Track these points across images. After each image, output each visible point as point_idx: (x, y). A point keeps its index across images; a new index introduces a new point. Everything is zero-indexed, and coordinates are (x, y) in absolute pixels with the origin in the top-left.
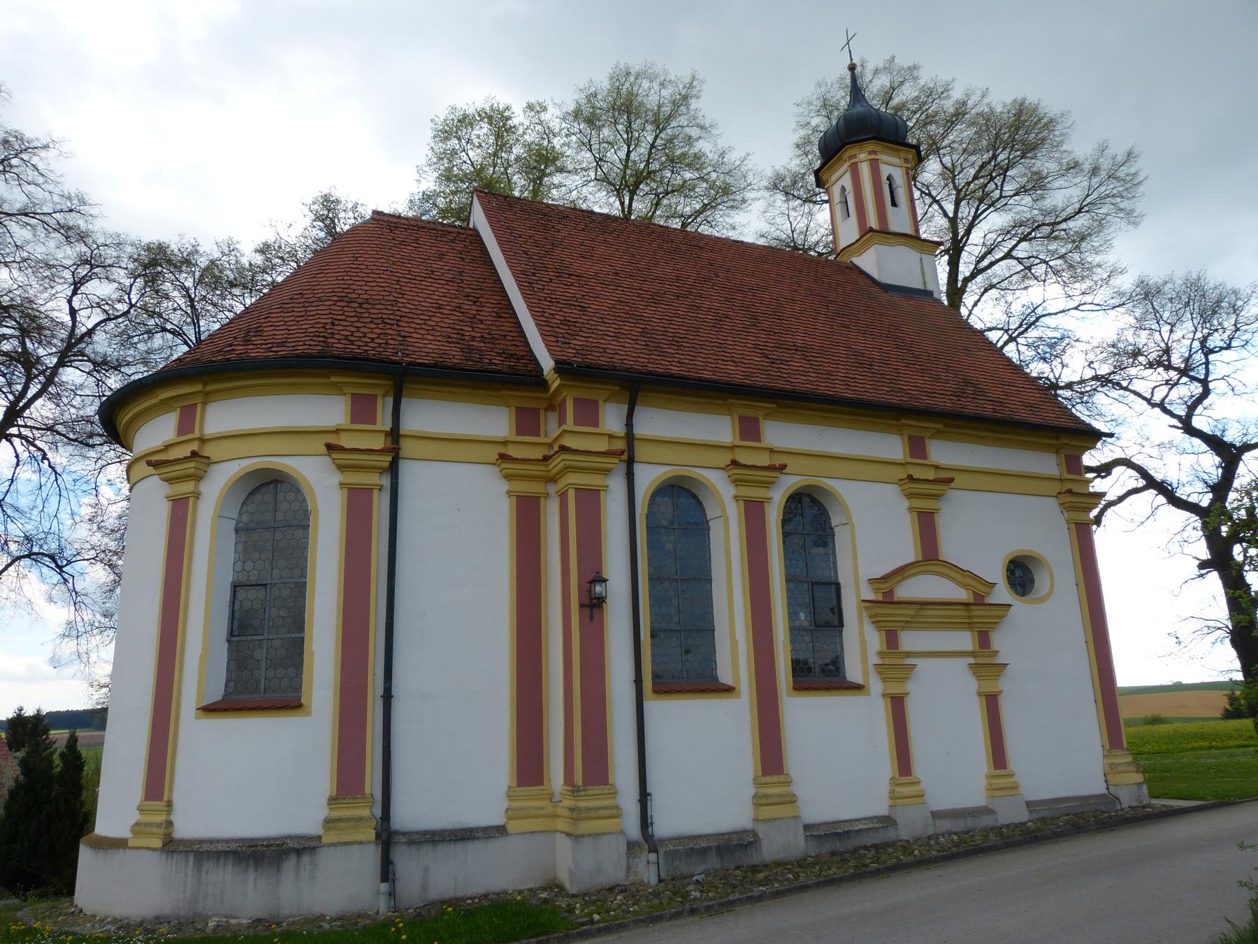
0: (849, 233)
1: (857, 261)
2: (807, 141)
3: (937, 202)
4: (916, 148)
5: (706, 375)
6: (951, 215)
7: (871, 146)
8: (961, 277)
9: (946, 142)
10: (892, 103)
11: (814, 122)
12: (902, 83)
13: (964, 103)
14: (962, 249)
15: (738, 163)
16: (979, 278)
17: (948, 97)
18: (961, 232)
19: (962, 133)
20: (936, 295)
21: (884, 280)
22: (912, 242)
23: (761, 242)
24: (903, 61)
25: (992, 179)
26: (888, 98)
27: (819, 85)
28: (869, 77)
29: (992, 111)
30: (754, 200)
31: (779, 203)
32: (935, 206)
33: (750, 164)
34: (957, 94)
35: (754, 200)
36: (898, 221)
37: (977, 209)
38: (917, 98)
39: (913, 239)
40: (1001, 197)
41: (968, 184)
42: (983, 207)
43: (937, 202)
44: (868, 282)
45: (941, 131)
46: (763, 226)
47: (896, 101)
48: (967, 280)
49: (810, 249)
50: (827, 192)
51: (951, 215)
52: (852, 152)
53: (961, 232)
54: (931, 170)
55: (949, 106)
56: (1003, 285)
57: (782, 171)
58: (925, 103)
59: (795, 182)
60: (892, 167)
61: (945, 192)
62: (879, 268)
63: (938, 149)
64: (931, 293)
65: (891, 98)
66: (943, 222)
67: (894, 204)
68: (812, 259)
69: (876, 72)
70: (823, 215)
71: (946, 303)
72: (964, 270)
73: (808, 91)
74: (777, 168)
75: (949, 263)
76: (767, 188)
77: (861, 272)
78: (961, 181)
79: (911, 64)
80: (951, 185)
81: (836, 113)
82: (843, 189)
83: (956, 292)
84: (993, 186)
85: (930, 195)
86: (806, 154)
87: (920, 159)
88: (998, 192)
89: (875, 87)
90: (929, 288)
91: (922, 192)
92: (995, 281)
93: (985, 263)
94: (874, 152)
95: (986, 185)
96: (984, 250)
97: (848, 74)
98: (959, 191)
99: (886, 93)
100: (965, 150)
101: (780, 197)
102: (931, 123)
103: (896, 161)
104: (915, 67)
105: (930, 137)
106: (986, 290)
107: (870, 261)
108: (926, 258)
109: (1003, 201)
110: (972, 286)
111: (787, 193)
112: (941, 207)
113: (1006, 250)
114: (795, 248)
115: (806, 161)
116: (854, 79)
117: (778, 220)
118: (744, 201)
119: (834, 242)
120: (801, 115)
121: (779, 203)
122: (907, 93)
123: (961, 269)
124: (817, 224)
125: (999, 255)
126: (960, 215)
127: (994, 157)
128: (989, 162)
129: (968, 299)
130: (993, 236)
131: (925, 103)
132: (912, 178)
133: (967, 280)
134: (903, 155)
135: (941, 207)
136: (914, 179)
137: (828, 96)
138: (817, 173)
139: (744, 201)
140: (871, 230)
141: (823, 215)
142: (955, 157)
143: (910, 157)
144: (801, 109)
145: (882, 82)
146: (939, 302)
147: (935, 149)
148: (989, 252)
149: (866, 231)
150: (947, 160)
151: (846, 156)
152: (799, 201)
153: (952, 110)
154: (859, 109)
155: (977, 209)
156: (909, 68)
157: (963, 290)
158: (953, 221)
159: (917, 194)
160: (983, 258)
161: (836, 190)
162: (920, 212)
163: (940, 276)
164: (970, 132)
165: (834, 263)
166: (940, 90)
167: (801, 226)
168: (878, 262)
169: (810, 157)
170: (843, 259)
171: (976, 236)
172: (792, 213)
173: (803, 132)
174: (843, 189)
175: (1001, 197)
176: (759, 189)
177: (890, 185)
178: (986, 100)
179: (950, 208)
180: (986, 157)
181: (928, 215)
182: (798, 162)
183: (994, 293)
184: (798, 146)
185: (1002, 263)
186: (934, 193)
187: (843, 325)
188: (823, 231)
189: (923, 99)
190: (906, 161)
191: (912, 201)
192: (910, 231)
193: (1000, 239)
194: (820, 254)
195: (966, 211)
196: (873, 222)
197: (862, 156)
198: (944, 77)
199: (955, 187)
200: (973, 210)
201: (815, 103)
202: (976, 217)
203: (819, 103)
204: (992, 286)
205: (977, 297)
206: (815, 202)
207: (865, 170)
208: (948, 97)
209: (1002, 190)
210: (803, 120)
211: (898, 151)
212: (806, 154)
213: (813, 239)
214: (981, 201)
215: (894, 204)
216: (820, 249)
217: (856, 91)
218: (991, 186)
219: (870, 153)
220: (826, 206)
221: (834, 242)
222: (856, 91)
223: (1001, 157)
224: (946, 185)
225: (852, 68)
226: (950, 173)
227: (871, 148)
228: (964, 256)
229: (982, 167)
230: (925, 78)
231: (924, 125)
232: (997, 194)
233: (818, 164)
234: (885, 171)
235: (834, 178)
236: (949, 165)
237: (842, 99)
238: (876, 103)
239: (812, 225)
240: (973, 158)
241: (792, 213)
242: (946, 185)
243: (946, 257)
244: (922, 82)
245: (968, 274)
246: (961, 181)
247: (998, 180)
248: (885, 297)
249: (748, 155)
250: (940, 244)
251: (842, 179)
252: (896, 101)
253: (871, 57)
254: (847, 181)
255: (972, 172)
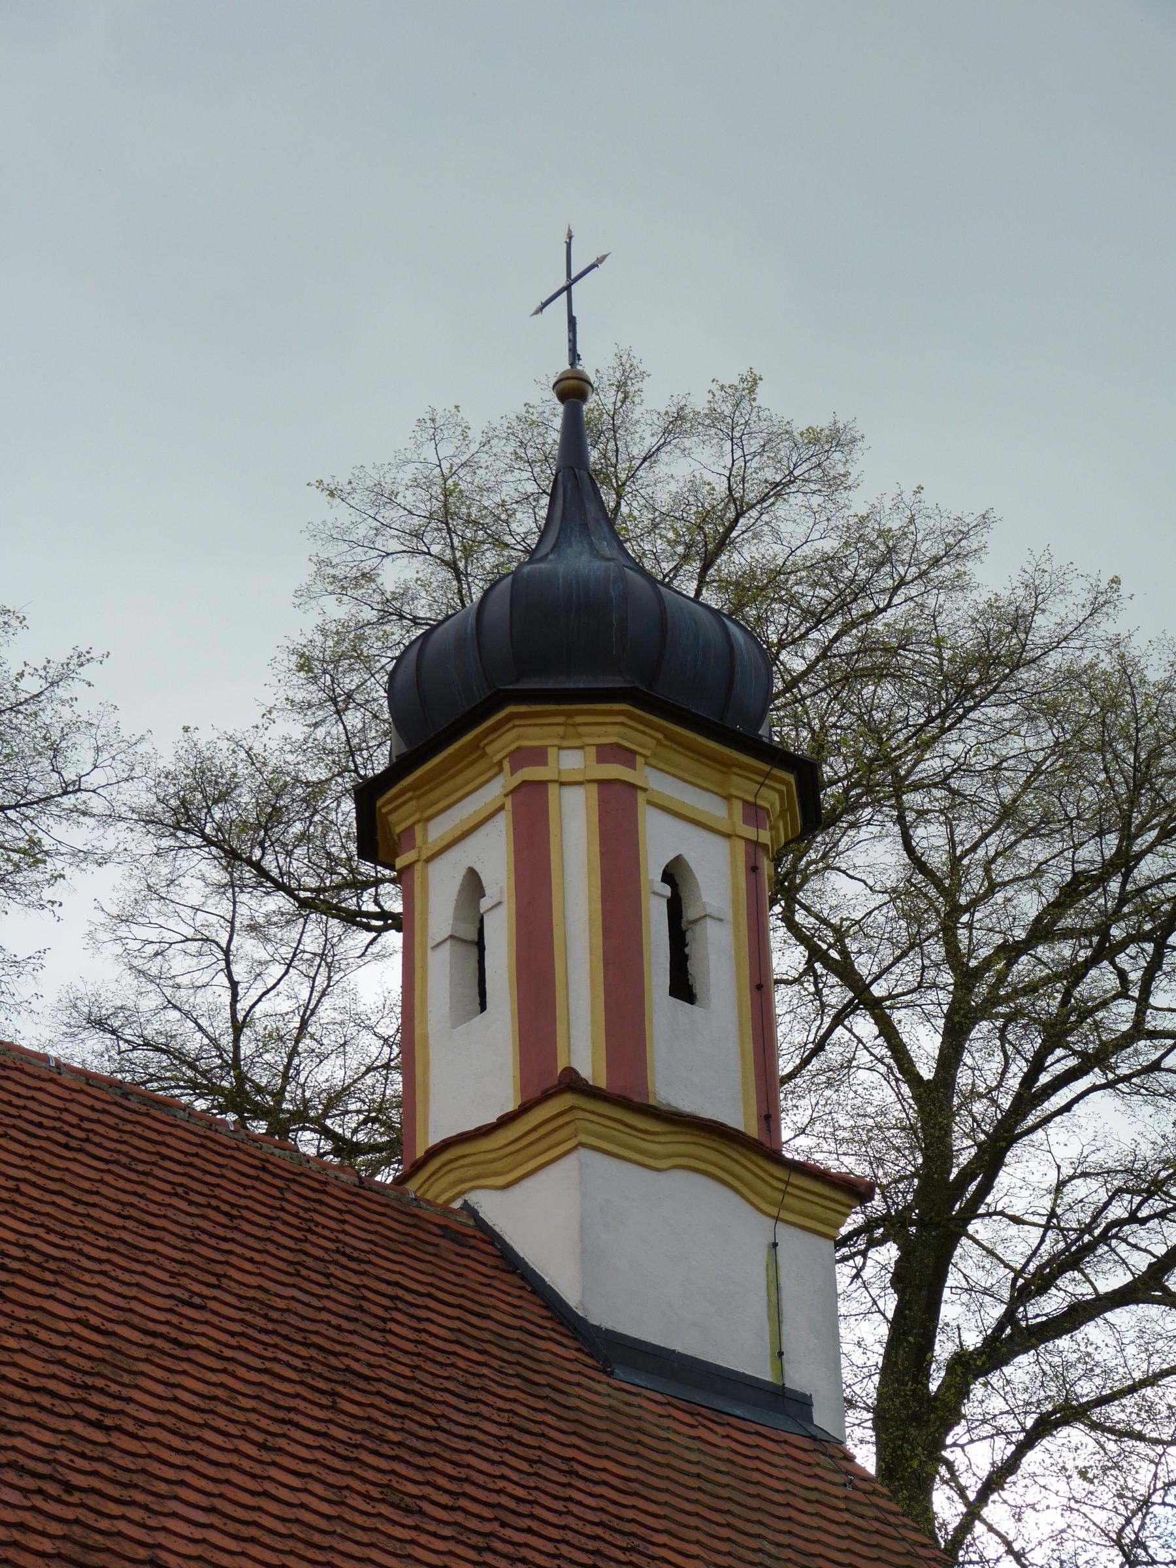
0: (474, 1080)
1: (498, 1209)
2: (349, 648)
3: (877, 1009)
4: (805, 772)
5: (740, 1075)
6: (926, 1072)
7: (613, 726)
8: (943, 1349)
9: (932, 764)
10: (733, 563)
11: (395, 574)
12: (777, 490)
13: (1020, 622)
14: (954, 1231)
15: (31, 685)
16: (1021, 1369)
17: (958, 584)
18: (965, 1152)
19: (999, 740)
20: (821, 1418)
21: (607, 1312)
22: (745, 1164)
23: (89, 1053)
24: (793, 404)
25: (1105, 951)
26: (712, 536)
27: (432, 427)
28: (641, 439)
29: (1125, 666)
30: (81, 856)
31: (193, 892)
32: (864, 1025)
33: (83, 699)
34: (994, 577)
35: (81, 856)
36: (694, 1063)
37: (1037, 1065)
38: (831, 563)
39: (746, 1151)
40: (1139, 1031)
41: (1010, 951)
42: (1059, 1062)
43: (877, 1009)
44: (534, 1311)
45: (916, 712)
46: (107, 979)
47: (745, 556)
48: (971, 1366)
49: (301, 1117)
50: (403, 878)
51: (926, 1072)
52: (529, 736)
53: (965, 1152)
54: (861, 870)
55: (958, 618)
56: (1115, 1413)
57: (223, 757)
58: (863, 590)
59: (273, 816)
60: (693, 831)
61: (907, 973)
62: (589, 1255)
63: (900, 787)
64: (801, 1404)
65: (723, 542)
66: (878, 1093)
67: (683, 987)
68: (301, 1172)
69: (677, 424)
70: (374, 978)
71: (866, 1458)
72: (963, 1321)
73: (384, 441)
74: (203, 738)
75: (900, 1279)
76: (149, 819)
77: (509, 1261)
78: (982, 935)
79: (823, 422)
80: (936, 950)
81: (490, 558)
82: (473, 885)
83: (917, 1411)
84: (1111, 982)
85: (845, 971)
86: (340, 703)
87: (813, 816)
88: (1126, 1008)
89: (665, 483)
90: (797, 1379)
91: (815, 954)
92: (1086, 1390)
93: (1051, 1304)
94: (626, 756)
95: (1076, 973)
96: (1053, 1245)
97: (555, 413)
98: (966, 978)
99: (706, 516)
100: (1007, 812)
101: (199, 870)
102: (878, 674)
103: (711, 807)
104: (836, 439)
105: (874, 731)
106: (1044, 1427)
107: (546, 1218)
108: (797, 1246)
109: (1147, 1051)
110: (984, 1399)
111: (232, 857)
112: (888, 1031)
113: (1141, 1262)
114: (240, 1098)
115: (331, 733)
116: (575, 432)
117: (179, 963)
118: (34, 854)
119: (409, 1100)
120: (339, 535)
121: (193, 892)
122: (791, 533)
123: (951, 1310)
124: (347, 1008)
125: (1112, 1280)
126: (964, 1078)
127: (1124, 861)
128: (1101, 880)
129: (972, 1454)
130: (1090, 1191)
131: (863, 590)
132: (777, 881)
133: (971, 1366)
134: (742, 787)
135: (888, 1031)
136: (787, 891)
137: (466, 481)
138: (368, 794)
139: (34, 854)
140: (572, 1083)
141: (374, 978)
142: (967, 832)
143: (771, 799)
144: (342, 514)
145: (686, 474)
146: (833, 1449)
147: (884, 781)
148: (1072, 1259)
149: (548, 1085)
150: (931, 837)
151: (502, 746)
152: (279, 902)
153: (967, 638)
154: (578, 562)
155: (1037, 1065)
156: (813, 437)
157: (946, 1411)
158: (934, 1099)
159: (786, 958)
160: (1039, 1282)
161: (442, 886)
162: (792, 1035)
163: (848, 1333)
164: (1033, 741)
165: (393, 1202)
166: (929, 549)
167: (278, 1007)
168: (589, 1232)
169: (354, 719)
170: (435, 1189)
171: (1023, 1179)
172: (247, 947)
173: (338, 610)
174: (473, 885)
175: (1139, 1031)
176: (112, 817)
177: (675, 908)
178: (1107, 627)
179: (924, 1043)
180: (1090, 854)
181: (833, 1054)
182: (298, 731)
183: (1073, 1438)
184: (305, 664)
185: (1120, 1316)
186: (864, 966)
187: (389, 1494)
188: (370, 1048)
189: (855, 568)
190: (754, 813)
191: (761, 986)
192: (736, 1114)
193: (1117, 1211)
194: (345, 1148)
195: (989, 1067)
196: (583, 1050)
197: (572, 762)
198: (950, 500)
199: (954, 958)
200: (1019, 1068)
201: (408, 498)
202: (1029, 1097)
203: (422, 503)
204: (1070, 1412)
205: (1003, 1450)
206: (353, 919)
207: (575, 822)
208: (958, 584)
209: (1143, 1003)
210: (347, 560)
211: (726, 766)
212: (340, 703)
213: (327, 1074)
214: (1055, 1034)
215: (683, 987)
216: (344, 1126)
217: (578, 487)
218: (1102, 979)
219: (606, 753)
220: (393, 939)
221: (409, 1100)
222: (578, 487)
223: (1149, 867)
224: (915, 944)
225: (573, 390)
226: (937, 897)
227: (611, 735)
228: (966, 1264)
229: (1071, 893)
230: (876, 486)
231: (851, 678)
232: (1122, 1013)
233: (380, 761)
234: (660, 840)
235: (439, 829)
236: (937, 860)
237: (519, 502)
238: (656, 552)
239: (326, 1012)
240: (1034, 851)
241: (247, 947)
242: (915, 944)
243: (889, 1253)
244: (858, 503)
245: (973, 1340)
246: (982, 935)
247: (1133, 961)
248: (600, 1392)
249: (83, 659)
250: (856, 1191)
251: (469, 843)
252: (745, 556)
253: (668, 354)
254: (492, 854)
255: (1029, 905)
